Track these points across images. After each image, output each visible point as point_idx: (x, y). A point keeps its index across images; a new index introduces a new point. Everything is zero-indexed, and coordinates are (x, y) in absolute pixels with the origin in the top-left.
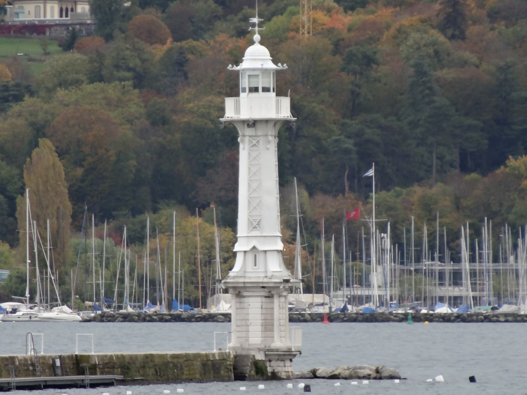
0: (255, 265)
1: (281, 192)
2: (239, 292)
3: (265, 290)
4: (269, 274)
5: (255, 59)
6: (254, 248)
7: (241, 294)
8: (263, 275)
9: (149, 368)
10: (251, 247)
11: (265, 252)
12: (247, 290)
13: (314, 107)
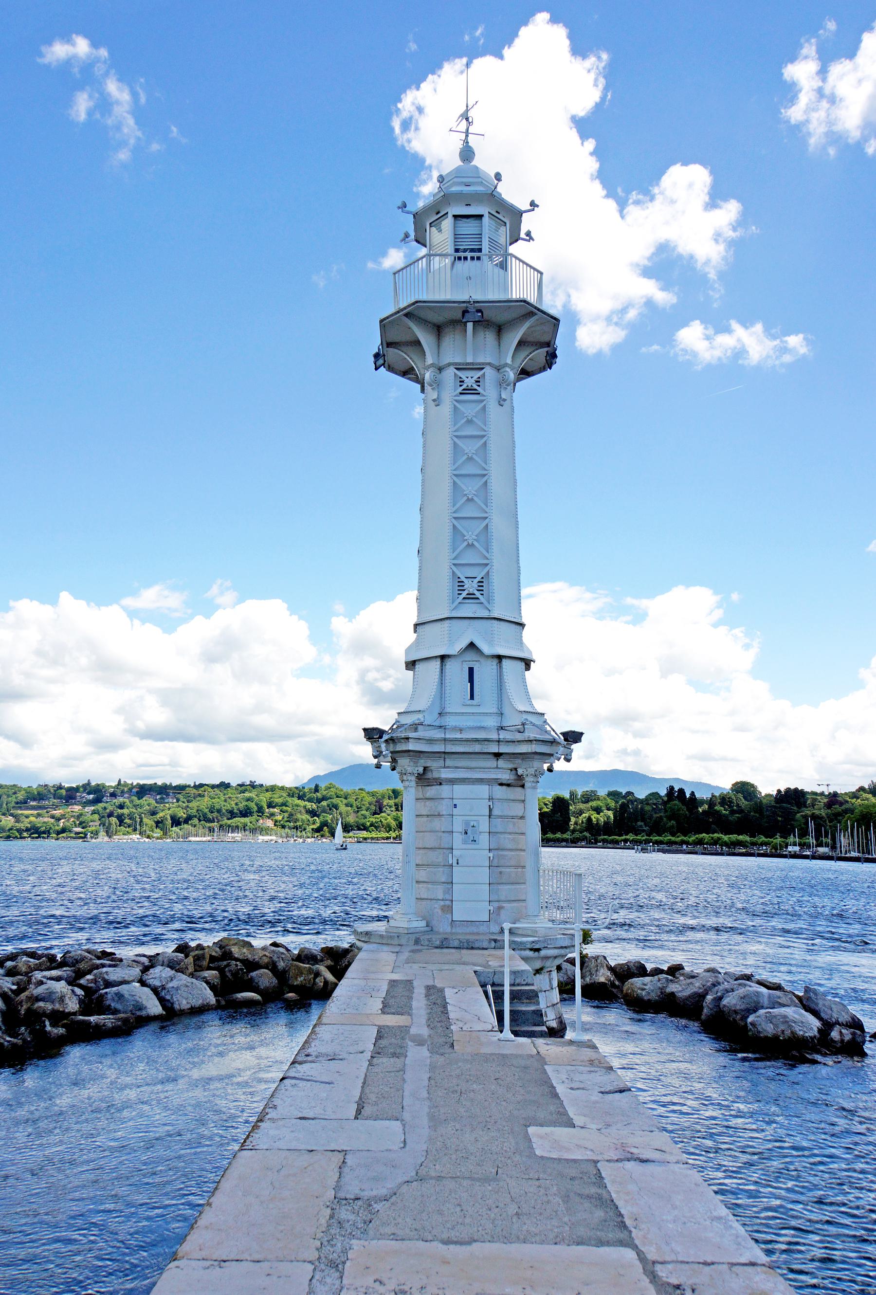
0: (472, 697)
1: (533, 375)
2: (425, 769)
3: (501, 763)
4: (512, 720)
5: (456, 767)
6: (472, 645)
7: (429, 775)
8: (492, 722)
9: (79, 1073)
10: (464, 643)
11: (500, 658)
12: (449, 763)
13: (709, 273)
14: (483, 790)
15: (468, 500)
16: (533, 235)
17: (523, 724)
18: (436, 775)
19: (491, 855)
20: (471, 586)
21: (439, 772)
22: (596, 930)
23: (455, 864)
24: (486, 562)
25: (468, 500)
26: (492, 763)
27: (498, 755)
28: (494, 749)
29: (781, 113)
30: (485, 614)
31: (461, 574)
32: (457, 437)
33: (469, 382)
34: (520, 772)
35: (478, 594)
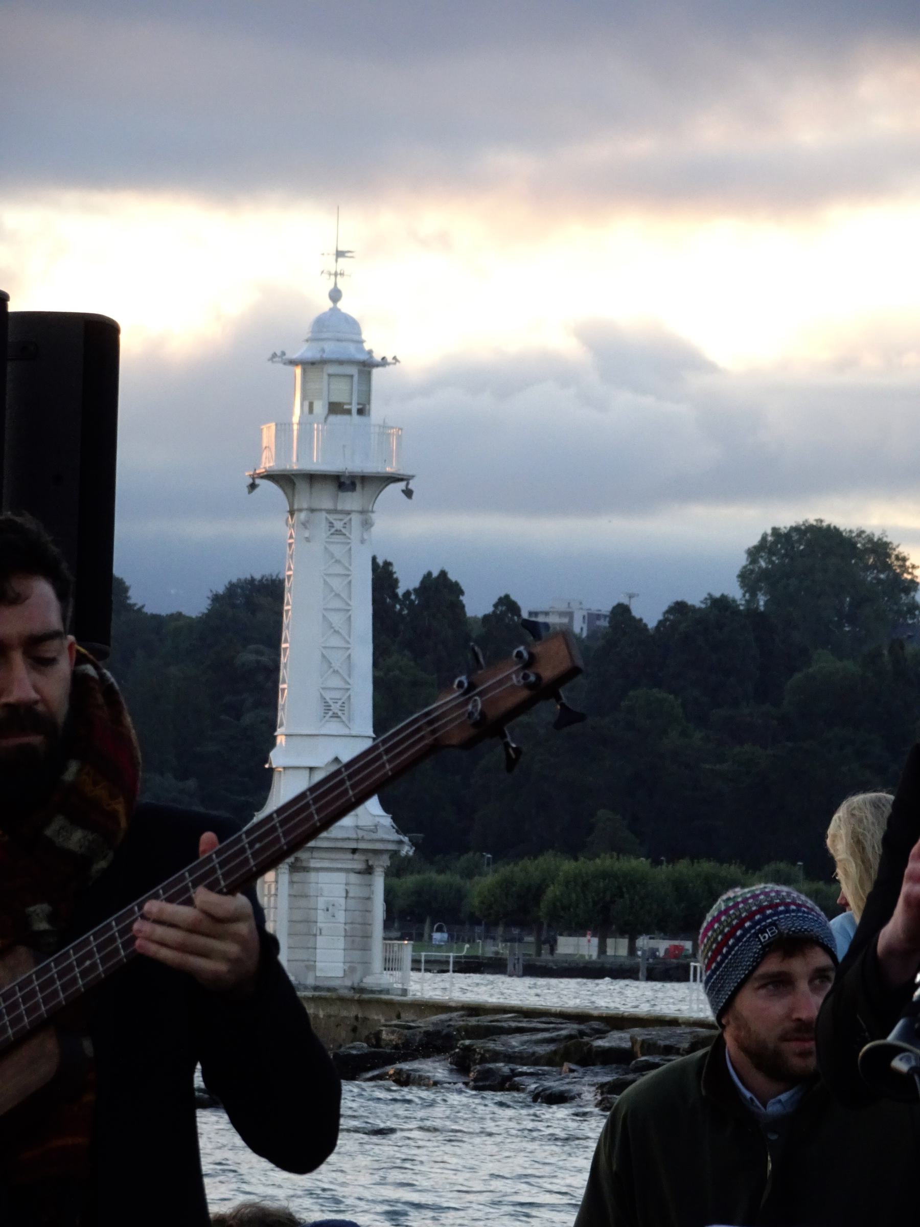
3: (356, 856)
7: (299, 864)
12: (315, 854)
14: (341, 877)
15: (334, 671)
16: (398, 358)
17: (376, 826)
18: (304, 864)
19: (347, 927)
20: (335, 708)
21: (309, 862)
22: (530, 955)
23: (318, 933)
24: (347, 573)
25: (334, 671)
26: (350, 856)
27: (354, 851)
28: (353, 845)
29: (413, 843)
30: (345, 731)
31: (328, 696)
32: (323, 689)
33: (338, 525)
34: (370, 863)
35: (340, 713)
